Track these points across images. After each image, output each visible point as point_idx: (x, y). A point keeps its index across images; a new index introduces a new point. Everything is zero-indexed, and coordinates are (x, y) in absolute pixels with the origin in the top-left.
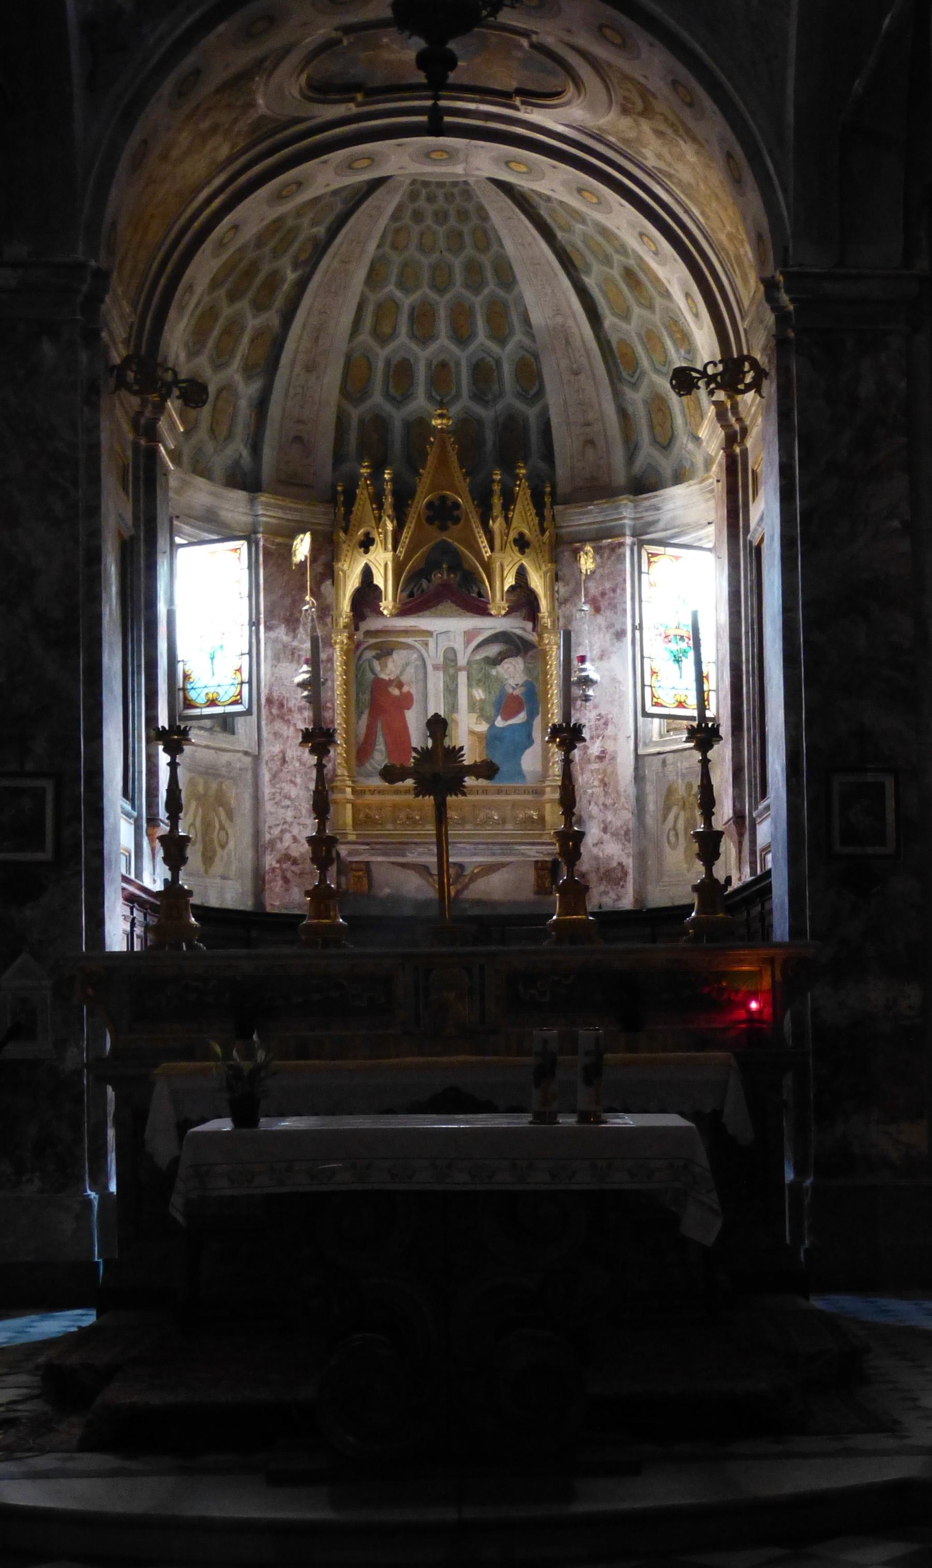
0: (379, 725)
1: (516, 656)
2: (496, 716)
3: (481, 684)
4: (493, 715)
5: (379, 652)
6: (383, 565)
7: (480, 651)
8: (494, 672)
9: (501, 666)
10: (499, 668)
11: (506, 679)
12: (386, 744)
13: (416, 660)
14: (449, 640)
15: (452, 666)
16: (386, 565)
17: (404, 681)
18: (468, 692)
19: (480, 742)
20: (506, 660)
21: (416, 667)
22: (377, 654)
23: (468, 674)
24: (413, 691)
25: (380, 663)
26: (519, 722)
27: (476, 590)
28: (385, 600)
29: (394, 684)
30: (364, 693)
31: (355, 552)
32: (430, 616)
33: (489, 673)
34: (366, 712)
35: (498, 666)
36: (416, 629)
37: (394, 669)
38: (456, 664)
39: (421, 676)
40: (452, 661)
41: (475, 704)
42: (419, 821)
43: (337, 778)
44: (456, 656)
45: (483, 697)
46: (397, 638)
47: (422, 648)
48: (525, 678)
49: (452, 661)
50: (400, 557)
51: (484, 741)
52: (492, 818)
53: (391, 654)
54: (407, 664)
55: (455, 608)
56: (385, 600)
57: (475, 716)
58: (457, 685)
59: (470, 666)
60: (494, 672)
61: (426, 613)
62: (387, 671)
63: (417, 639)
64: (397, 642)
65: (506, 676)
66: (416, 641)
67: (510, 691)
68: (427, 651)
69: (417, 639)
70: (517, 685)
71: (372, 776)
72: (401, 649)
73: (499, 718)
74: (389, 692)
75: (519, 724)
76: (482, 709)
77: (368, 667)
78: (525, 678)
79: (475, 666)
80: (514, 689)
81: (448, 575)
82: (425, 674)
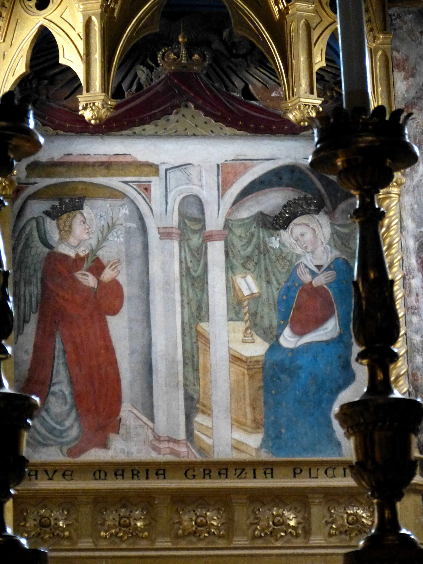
0: (59, 345)
1: (317, 212)
2: (281, 328)
3: (251, 265)
4: (275, 323)
5: (57, 203)
6: (80, 28)
7: (249, 204)
8: (275, 243)
9: (289, 230)
10: (285, 234)
11: (298, 256)
12: (72, 382)
13: (128, 218)
14: (189, 181)
15: (195, 232)
16: (88, 24)
17: (105, 261)
18: (227, 280)
19: (251, 377)
20: (296, 221)
21: (128, 231)
22: (53, 207)
23: (226, 246)
24: (122, 279)
25: (58, 226)
26: (324, 338)
27: (239, 84)
28: (88, 91)
29: (86, 266)
30: (28, 283)
31: (18, 8)
32: (156, 135)
33: (265, 244)
34: (34, 319)
35: (282, 232)
36: (128, 159)
37: (86, 237)
38: (204, 226)
39: (138, 248)
40: (195, 220)
41: (240, 303)
42: (142, 530)
43: (396, 274)
44: (202, 211)
45: (255, 290)
46: (89, 176)
47: (139, 197)
48: (336, 253)
49: (195, 220)
50: (113, 10)
51: (259, 376)
52: (284, 523)
53: (80, 208)
54: (111, 227)
55: (202, 117)
56: (88, 91)
57: (241, 326)
58: (206, 265)
59: (230, 230)
60: (275, 243)
61: (149, 128)
62: (73, 241)
63: (128, 179)
64: (92, 184)
65: (299, 251)
66: (126, 183)
67: (307, 278)
68: (148, 202)
69: (128, 179)
70: (319, 267)
71: (45, 445)
72: (95, 197)
73: (287, 331)
74: (75, 280)
75: (327, 342)
76: (254, 315)
77: (35, 233)
78: (336, 253)
79: (238, 231)
80: (313, 274)
81: (190, 56)
82: (146, 246)
